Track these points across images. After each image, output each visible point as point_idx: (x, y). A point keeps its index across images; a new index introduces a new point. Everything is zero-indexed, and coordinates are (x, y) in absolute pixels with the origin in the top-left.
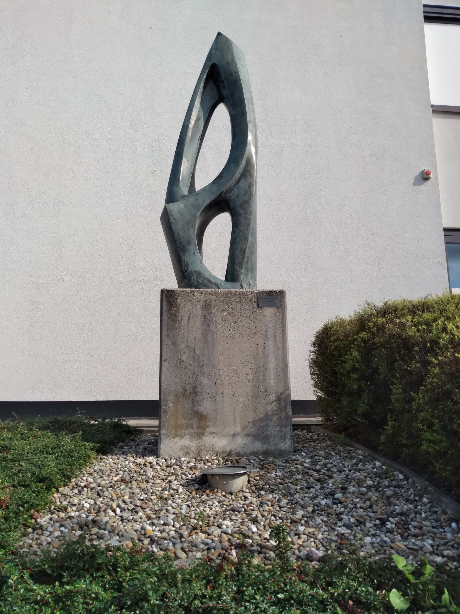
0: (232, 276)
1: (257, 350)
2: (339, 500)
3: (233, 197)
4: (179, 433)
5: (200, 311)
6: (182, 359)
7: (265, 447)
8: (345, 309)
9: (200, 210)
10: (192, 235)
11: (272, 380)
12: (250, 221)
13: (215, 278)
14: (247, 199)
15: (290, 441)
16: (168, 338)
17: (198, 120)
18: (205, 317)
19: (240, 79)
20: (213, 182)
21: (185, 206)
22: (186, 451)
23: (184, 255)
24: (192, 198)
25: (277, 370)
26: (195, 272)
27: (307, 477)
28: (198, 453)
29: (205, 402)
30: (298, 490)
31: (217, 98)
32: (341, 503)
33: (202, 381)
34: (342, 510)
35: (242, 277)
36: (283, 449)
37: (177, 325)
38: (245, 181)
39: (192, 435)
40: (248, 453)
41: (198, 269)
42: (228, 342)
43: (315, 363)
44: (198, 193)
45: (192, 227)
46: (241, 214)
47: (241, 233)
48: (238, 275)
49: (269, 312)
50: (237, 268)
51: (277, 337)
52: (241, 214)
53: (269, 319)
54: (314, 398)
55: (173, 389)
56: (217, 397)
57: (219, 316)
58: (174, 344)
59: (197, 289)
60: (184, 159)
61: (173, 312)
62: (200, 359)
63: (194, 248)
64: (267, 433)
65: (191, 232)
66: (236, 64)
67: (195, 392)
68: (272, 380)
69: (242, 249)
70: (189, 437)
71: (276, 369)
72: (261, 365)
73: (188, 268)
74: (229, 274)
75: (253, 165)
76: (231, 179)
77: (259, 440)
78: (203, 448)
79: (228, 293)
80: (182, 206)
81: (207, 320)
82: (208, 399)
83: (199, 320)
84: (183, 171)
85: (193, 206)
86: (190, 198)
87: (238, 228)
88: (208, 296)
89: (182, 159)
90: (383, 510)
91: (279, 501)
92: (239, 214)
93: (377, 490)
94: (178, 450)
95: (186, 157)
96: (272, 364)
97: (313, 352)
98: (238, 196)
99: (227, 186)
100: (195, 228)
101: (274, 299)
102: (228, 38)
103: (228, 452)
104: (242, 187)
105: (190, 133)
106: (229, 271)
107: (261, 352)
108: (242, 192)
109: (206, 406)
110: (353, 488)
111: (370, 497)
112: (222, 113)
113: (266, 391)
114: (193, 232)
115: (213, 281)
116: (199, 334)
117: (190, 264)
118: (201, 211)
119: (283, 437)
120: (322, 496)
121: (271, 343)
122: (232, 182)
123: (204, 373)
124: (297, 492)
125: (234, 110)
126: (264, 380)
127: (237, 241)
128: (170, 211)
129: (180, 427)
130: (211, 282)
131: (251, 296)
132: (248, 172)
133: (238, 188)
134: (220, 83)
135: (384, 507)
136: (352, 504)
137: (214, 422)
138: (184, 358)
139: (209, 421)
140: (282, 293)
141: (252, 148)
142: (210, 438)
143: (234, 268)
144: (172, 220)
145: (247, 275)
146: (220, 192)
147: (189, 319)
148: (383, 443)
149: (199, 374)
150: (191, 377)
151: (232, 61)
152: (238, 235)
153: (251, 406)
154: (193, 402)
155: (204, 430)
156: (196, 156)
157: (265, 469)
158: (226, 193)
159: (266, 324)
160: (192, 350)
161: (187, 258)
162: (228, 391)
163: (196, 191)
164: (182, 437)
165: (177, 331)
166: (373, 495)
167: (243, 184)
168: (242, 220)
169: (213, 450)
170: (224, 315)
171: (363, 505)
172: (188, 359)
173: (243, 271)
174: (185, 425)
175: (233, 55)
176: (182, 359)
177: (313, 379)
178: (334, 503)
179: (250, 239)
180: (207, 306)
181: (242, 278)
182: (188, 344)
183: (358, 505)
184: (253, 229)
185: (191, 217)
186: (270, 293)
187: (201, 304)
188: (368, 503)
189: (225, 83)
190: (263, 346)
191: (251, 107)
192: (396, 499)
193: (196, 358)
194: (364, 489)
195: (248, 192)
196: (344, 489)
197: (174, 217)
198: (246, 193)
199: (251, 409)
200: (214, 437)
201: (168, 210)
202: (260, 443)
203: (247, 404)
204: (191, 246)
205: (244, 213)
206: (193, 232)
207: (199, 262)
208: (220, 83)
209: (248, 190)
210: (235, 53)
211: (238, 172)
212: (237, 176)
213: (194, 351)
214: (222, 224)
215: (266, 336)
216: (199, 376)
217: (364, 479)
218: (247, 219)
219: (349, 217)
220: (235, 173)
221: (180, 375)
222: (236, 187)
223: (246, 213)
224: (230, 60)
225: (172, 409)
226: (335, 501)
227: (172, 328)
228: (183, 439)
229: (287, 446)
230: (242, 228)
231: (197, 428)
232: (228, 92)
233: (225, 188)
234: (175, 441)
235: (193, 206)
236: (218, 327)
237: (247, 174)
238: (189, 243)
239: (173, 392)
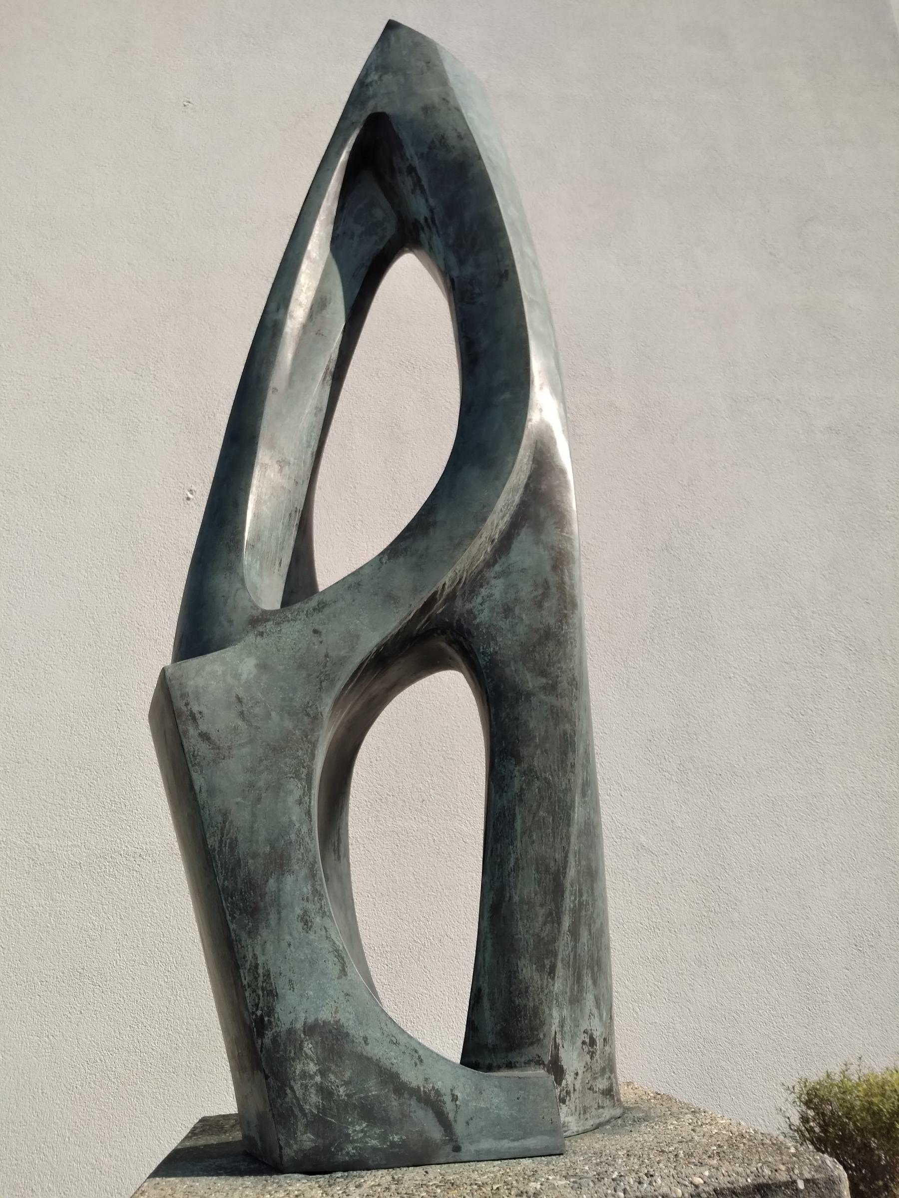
0: (501, 1028)
3: (484, 617)
9: (333, 682)
10: (296, 813)
12: (573, 725)
14: (552, 621)
17: (319, 304)
19: (480, 158)
20: (395, 550)
21: (263, 667)
23: (253, 933)
24: (298, 625)
26: (311, 1029)
31: (390, 229)
35: (555, 1017)
38: (537, 542)
41: (325, 1015)
44: (324, 591)
45: (297, 776)
46: (529, 695)
47: (537, 784)
48: (536, 1012)
50: (527, 971)
52: (529, 695)
60: (264, 457)
63: (307, 889)
65: (291, 800)
66: (458, 109)
69: (547, 870)
73: (271, 1011)
74: (486, 1003)
75: (563, 472)
76: (473, 535)
80: (248, 667)
84: (258, 503)
85: (301, 666)
86: (286, 628)
87: (519, 760)
89: (253, 453)
92: (521, 696)
95: (272, 446)
98: (508, 611)
99: (459, 566)
100: (309, 778)
102: (423, 37)
104: (523, 570)
105: (287, 353)
106: (486, 989)
108: (526, 591)
112: (412, 288)
114: (300, 802)
115: (411, 1076)
117: (281, 985)
118: (340, 685)
122: (480, 547)
125: (461, 262)
127: (518, 825)
128: (184, 696)
132: (540, 502)
133: (505, 573)
134: (404, 180)
141: (544, 409)
143: (512, 975)
144: (192, 741)
145: (576, 1000)
146: (425, 596)
151: (445, 101)
152: (520, 797)
156: (314, 444)
158: (452, 597)
163: (321, 588)
167: (524, 552)
168: (535, 722)
173: (558, 986)
175: (443, 81)
179: (578, 815)
181: (555, 1027)
184: (588, 761)
185: (288, 724)
189: (422, 174)
191: (527, 250)
195: (553, 590)
197: (203, 727)
198: (545, 595)
201: (176, 693)
204: (289, 879)
205: (544, 688)
206: (300, 802)
207: (335, 970)
208: (404, 180)
209: (552, 579)
210: (451, 78)
211: (500, 503)
212: (497, 520)
214: (434, 725)
218: (559, 715)
219: (795, 611)
220: (488, 507)
222: (497, 568)
223: (552, 688)
224: (436, 100)
230: (538, 763)
232: (432, 202)
233: (448, 578)
235: (301, 666)
237: (543, 512)
238: (279, 862)
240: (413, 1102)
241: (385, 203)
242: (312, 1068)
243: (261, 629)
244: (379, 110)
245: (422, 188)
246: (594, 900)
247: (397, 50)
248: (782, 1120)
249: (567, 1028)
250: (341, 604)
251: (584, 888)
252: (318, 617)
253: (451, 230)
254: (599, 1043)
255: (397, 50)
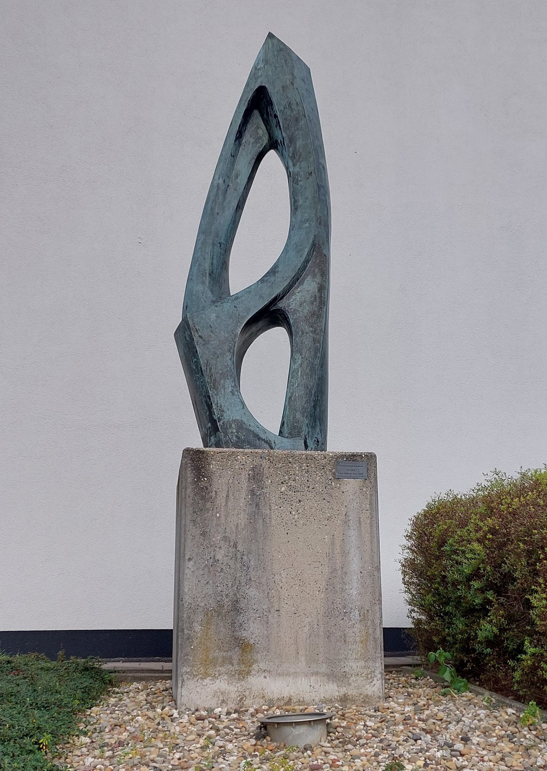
1: (333, 544)
2: (460, 752)
4: (210, 671)
5: (245, 485)
6: (217, 558)
7: (343, 690)
8: (465, 480)
11: (354, 589)
13: (265, 431)
15: (380, 681)
16: (195, 525)
18: (252, 492)
20: (262, 280)
22: (221, 698)
24: (229, 304)
25: (362, 575)
27: (411, 728)
28: (240, 701)
29: (251, 624)
30: (401, 742)
31: (265, 140)
32: (462, 755)
33: (247, 591)
34: (466, 763)
36: (370, 693)
37: (208, 505)
39: (231, 675)
40: (317, 699)
42: (288, 531)
43: (410, 567)
44: (237, 297)
49: (351, 485)
51: (363, 525)
53: (351, 497)
54: (408, 624)
55: (203, 604)
56: (270, 616)
57: (273, 491)
58: (204, 534)
59: (241, 450)
61: (202, 484)
62: (245, 558)
64: (346, 669)
67: (236, 608)
68: (354, 589)
70: (226, 677)
71: (361, 572)
72: (338, 566)
74: (285, 425)
77: (333, 681)
78: (247, 693)
79: (287, 456)
81: (256, 498)
82: (255, 619)
83: (244, 496)
88: (257, 461)
90: (520, 763)
91: (376, 755)
93: (510, 741)
94: (209, 698)
96: (355, 564)
97: (408, 548)
101: (360, 466)
103: (286, 700)
106: (286, 421)
107: (338, 547)
109: (253, 631)
110: (478, 739)
111: (502, 749)
113: (344, 607)
114: (231, 359)
115: (263, 436)
116: (243, 519)
119: (369, 676)
120: (435, 748)
121: (353, 533)
123: (250, 579)
124: (400, 745)
126: (343, 590)
129: (214, 662)
130: (259, 439)
131: (323, 462)
134: (272, 115)
135: (522, 759)
136: (477, 757)
137: (265, 653)
138: (219, 557)
139: (257, 652)
140: (371, 458)
142: (259, 678)
147: (227, 496)
148: (518, 682)
149: (243, 581)
150: (230, 585)
153: (322, 629)
154: (233, 623)
155: (250, 666)
157: (347, 719)
159: (345, 504)
160: (232, 544)
161: (220, 399)
162: (286, 606)
164: (215, 677)
165: (209, 515)
166: (506, 747)
169: (264, 697)
170: (283, 489)
171: (492, 758)
172: (226, 558)
174: (220, 660)
176: (217, 558)
177: (409, 591)
178: (453, 756)
180: (256, 476)
182: (226, 535)
183: (486, 758)
186: (353, 457)
187: (246, 473)
188: (499, 755)
190: (341, 538)
192: (537, 750)
193: (239, 556)
194: (494, 740)
196: (466, 740)
199: (322, 634)
200: (265, 677)
202: (335, 685)
203: (315, 626)
206: (231, 359)
208: (272, 115)
213: (235, 546)
215: (346, 522)
216: (243, 584)
217: (493, 728)
221: (214, 583)
225: (199, 635)
226: (453, 753)
227: (202, 510)
228: (218, 681)
229: (375, 689)
231: (239, 664)
234: (204, 684)
236: (273, 508)
239: (201, 609)
240: (263, 442)
241: (263, 126)
242: (234, 431)
243: (216, 304)
244: (263, 85)
245: (280, 126)
246: (322, 400)
247: (276, 51)
248: (411, 619)
249: (310, 434)
250: (244, 298)
251: (319, 396)
252: (235, 302)
253: (291, 149)
254: (320, 443)
255: (276, 51)
